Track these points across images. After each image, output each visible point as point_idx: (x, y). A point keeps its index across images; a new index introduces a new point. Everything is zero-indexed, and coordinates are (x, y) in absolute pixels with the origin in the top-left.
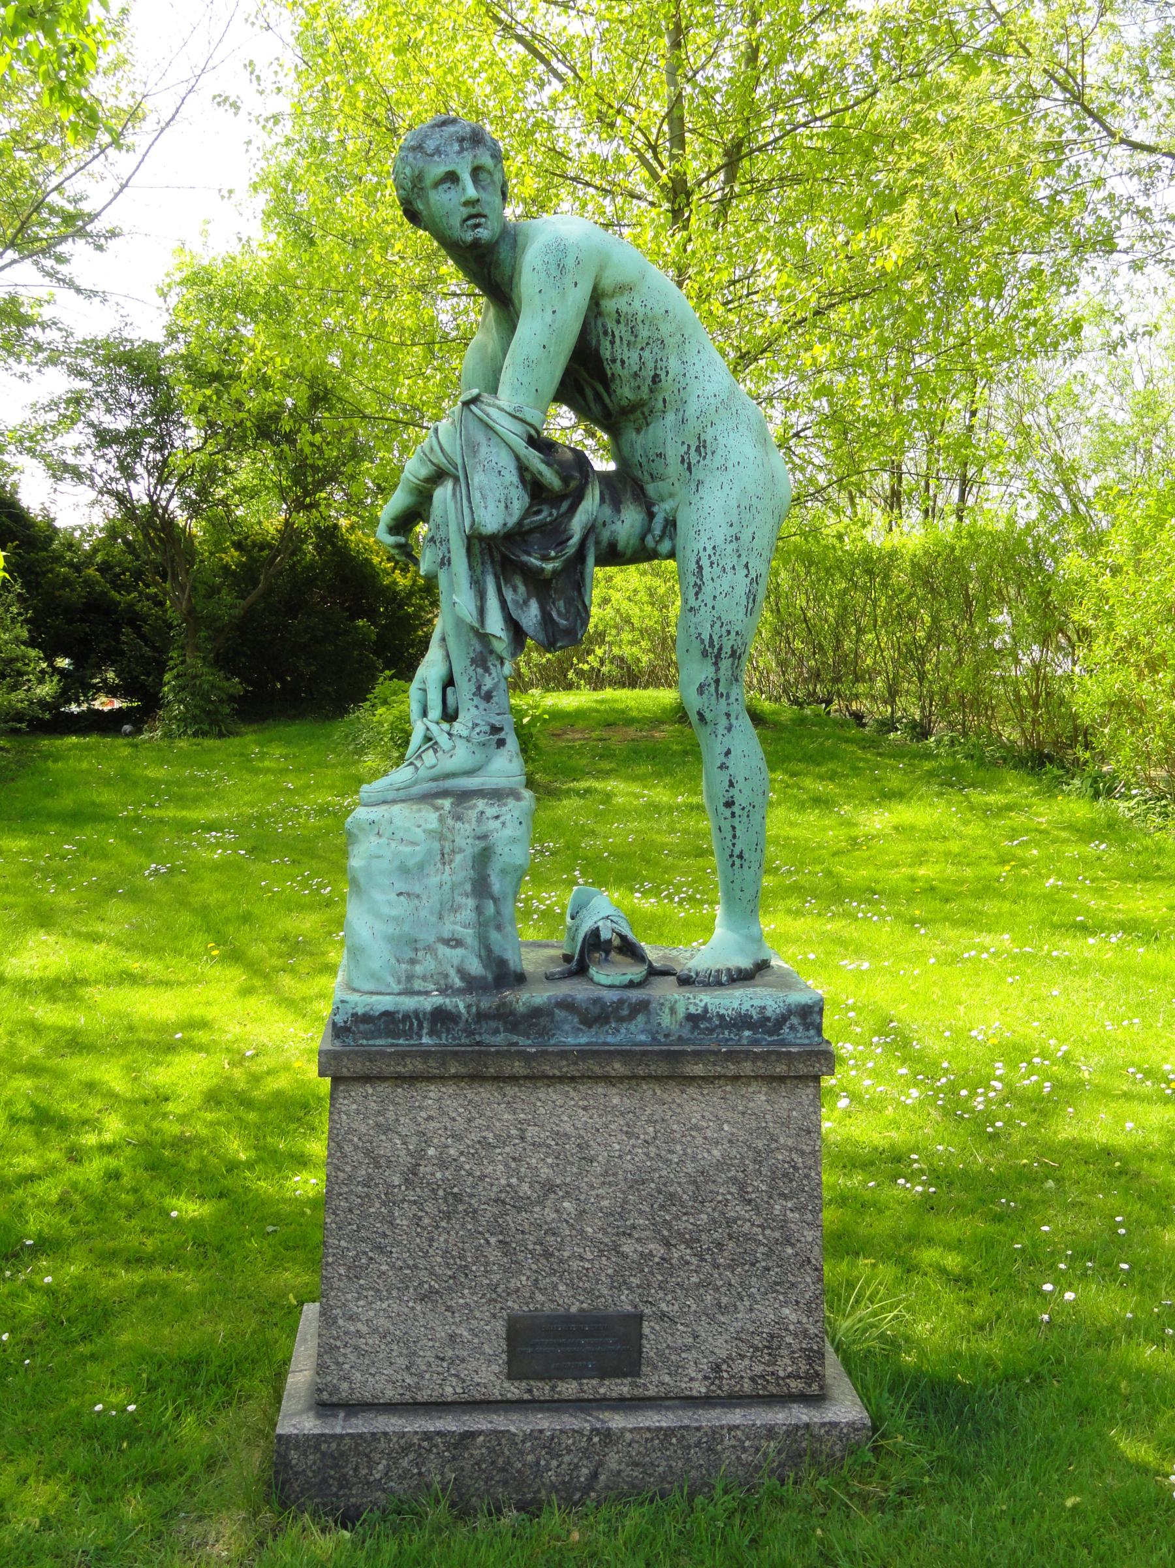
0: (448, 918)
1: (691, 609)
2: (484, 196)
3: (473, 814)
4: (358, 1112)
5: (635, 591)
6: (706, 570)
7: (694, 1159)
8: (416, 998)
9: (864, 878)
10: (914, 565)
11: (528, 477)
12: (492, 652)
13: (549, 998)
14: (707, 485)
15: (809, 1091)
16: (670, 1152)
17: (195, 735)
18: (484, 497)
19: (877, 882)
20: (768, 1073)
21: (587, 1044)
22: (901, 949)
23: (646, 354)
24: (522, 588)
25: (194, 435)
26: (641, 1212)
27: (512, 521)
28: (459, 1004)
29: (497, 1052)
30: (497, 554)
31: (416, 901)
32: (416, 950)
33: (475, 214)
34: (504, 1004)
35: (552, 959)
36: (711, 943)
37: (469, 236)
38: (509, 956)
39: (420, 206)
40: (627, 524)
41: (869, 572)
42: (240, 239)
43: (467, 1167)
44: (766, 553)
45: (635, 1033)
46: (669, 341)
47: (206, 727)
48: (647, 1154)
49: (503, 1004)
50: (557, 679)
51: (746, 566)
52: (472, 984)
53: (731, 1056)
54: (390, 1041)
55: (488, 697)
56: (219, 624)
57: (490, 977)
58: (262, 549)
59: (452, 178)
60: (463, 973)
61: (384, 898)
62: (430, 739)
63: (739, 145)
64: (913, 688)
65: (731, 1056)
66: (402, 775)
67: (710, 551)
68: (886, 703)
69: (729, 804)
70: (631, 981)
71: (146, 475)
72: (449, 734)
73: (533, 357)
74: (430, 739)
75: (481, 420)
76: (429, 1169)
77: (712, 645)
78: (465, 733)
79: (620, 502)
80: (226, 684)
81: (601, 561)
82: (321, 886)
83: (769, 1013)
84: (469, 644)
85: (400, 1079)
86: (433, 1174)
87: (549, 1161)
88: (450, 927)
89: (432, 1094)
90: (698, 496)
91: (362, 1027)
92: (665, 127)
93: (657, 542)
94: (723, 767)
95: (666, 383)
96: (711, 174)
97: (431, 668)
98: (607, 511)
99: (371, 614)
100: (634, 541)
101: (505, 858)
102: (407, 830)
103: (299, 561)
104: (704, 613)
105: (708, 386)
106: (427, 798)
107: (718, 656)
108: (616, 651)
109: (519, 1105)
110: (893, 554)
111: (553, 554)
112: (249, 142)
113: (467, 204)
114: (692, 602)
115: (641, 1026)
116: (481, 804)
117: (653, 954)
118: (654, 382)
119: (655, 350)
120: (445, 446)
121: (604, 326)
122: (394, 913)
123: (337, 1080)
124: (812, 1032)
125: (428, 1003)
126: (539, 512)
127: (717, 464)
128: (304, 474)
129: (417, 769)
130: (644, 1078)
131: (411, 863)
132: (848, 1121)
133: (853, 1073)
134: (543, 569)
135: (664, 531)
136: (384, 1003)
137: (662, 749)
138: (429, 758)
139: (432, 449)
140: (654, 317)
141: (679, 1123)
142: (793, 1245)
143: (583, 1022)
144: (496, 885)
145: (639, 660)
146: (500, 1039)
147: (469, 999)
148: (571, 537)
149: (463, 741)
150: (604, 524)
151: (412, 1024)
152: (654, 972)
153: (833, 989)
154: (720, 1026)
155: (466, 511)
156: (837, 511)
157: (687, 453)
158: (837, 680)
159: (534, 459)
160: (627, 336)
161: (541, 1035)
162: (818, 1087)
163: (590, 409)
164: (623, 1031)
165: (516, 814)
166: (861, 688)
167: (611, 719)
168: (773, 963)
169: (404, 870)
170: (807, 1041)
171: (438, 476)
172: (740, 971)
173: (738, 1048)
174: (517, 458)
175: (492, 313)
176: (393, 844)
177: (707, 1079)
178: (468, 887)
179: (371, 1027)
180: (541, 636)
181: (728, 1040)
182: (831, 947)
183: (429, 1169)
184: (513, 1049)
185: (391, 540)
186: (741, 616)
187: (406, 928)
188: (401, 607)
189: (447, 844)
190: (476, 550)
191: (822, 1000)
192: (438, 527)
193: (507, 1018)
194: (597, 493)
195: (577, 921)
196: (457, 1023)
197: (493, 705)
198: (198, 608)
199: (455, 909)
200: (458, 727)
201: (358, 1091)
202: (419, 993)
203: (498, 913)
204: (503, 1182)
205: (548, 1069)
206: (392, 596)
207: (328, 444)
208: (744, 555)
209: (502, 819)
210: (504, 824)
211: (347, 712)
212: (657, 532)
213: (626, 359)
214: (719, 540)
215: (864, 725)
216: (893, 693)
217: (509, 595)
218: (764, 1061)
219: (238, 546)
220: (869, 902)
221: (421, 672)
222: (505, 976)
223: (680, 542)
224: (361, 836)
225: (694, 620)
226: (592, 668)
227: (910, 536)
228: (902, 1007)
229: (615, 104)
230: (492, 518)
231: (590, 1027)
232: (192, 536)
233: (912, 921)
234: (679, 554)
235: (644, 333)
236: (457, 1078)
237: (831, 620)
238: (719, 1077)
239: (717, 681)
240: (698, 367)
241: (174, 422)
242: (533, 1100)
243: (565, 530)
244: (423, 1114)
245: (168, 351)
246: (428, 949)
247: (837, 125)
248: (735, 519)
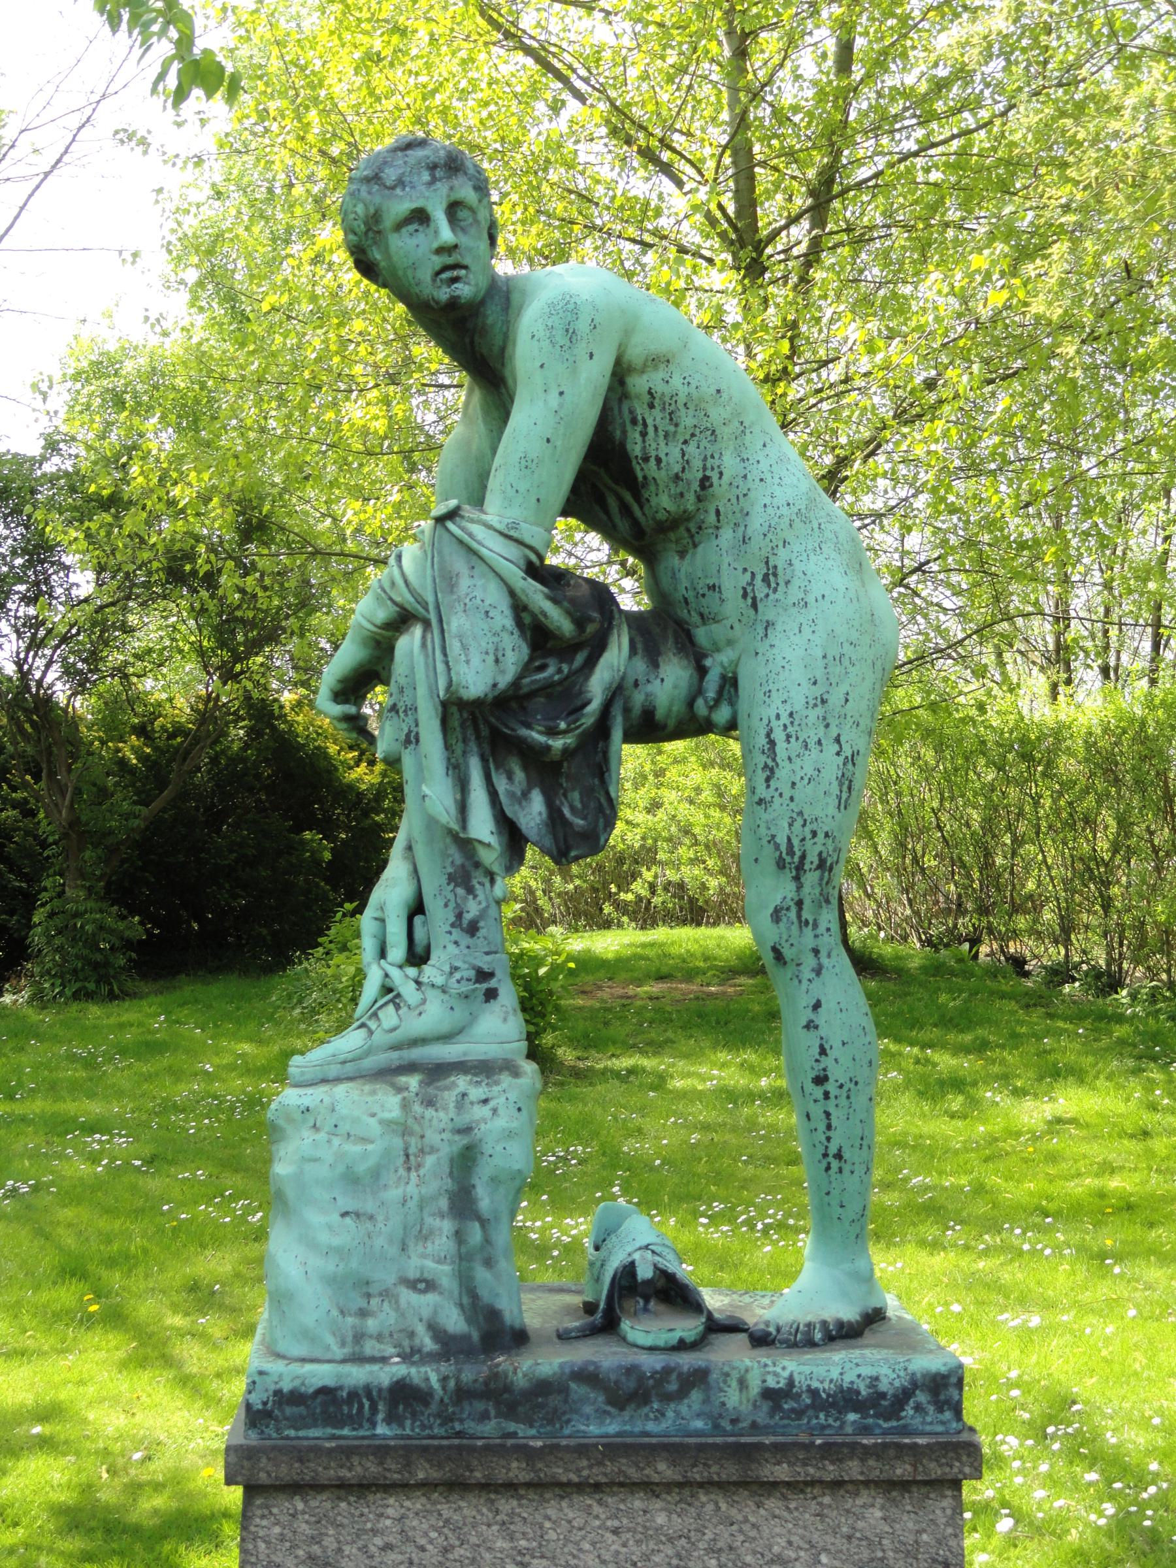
0: (415, 1249)
1: (760, 802)
2: (464, 240)
3: (450, 1097)
4: (282, 1538)
5: (698, 790)
6: (781, 746)
8: (368, 1367)
9: (1031, 1194)
10: (1088, 746)
11: (527, 619)
12: (477, 865)
13: (561, 1366)
14: (779, 627)
17: (76, 996)
18: (465, 648)
19: (1050, 1199)
20: (884, 1476)
21: (619, 1434)
22: (1086, 1297)
23: (691, 449)
24: (520, 775)
25: (84, 583)
27: (505, 681)
28: (430, 1376)
29: (487, 1448)
30: (484, 726)
31: (369, 1225)
32: (369, 1296)
33: (452, 265)
34: (496, 1375)
35: (568, 1311)
36: (795, 1283)
37: (443, 294)
38: (504, 1305)
39: (376, 255)
40: (669, 683)
41: (1026, 757)
42: (147, 319)
44: (865, 722)
45: (686, 1417)
46: (725, 432)
47: (91, 986)
49: (495, 1376)
50: (587, 912)
51: (838, 740)
52: (450, 1347)
53: (830, 1451)
54: (330, 1431)
55: (472, 929)
56: (110, 840)
57: (475, 1336)
58: (172, 736)
59: (420, 217)
60: (435, 1330)
61: (321, 1219)
62: (390, 990)
63: (830, 182)
64: (1094, 921)
65: (830, 1451)
66: (351, 1041)
67: (785, 719)
68: (1056, 942)
69: (820, 1080)
70: (681, 1341)
71: (14, 637)
72: (418, 982)
73: (533, 455)
74: (390, 990)
75: (461, 542)
77: (791, 852)
78: (439, 980)
79: (659, 654)
80: (121, 925)
81: (631, 737)
82: (248, 1211)
83: (884, 1386)
84: (444, 855)
85: (343, 1488)
88: (419, 1262)
90: (767, 642)
91: (289, 1410)
92: (727, 160)
93: (711, 709)
94: (810, 1026)
95: (720, 488)
96: (793, 220)
97: (391, 890)
98: (640, 666)
99: (327, 828)
100: (678, 708)
101: (498, 1160)
102: (356, 1121)
103: (223, 752)
104: (779, 807)
105: (778, 491)
106: (386, 1074)
107: (800, 868)
108: (672, 875)
109: (518, 1527)
110: (1059, 732)
111: (563, 725)
112: (160, 191)
113: (440, 251)
114: (762, 791)
115: (696, 1407)
116: (462, 1082)
117: (713, 1300)
119: (704, 443)
120: (412, 578)
121: (631, 412)
122: (336, 1241)
123: (252, 1491)
124: (948, 1415)
125: (385, 1375)
126: (543, 668)
127: (792, 599)
128: (233, 632)
129: (371, 1032)
130: (701, 1485)
131: (361, 1168)
132: (1013, 1553)
133: (1019, 1480)
134: (548, 748)
135: (720, 692)
136: (321, 1374)
137: (733, 1009)
138: (389, 1016)
139: (393, 584)
140: (702, 399)
141: (755, 1553)
143: (610, 1402)
144: (485, 1200)
145: (704, 887)
146: (489, 1428)
147: (446, 1368)
148: (588, 702)
149: (437, 992)
150: (636, 684)
151: (361, 1406)
152: (718, 1327)
153: (987, 1355)
154: (813, 1406)
155: (440, 667)
156: (980, 672)
157: (751, 584)
158: (984, 910)
159: (536, 594)
160: (664, 425)
161: (551, 1422)
162: (958, 1498)
163: (614, 526)
164: (670, 1414)
165: (513, 1096)
166: (1022, 922)
167: (665, 970)
168: (890, 1313)
169: (351, 1179)
170: (940, 1428)
171: (402, 620)
172: (840, 1324)
173: (839, 1439)
174: (512, 593)
175: (477, 396)
176: (336, 1141)
177: (795, 1487)
178: (444, 1203)
179: (302, 1410)
180: (548, 842)
182: (983, 1295)
184: (510, 1442)
185: (338, 709)
186: (832, 810)
187: (354, 1264)
188: (366, 814)
189: (413, 1141)
190: (455, 722)
191: (961, 1366)
192: (401, 690)
193: (500, 1396)
194: (625, 641)
195: (603, 1253)
196: (427, 1404)
197: (479, 941)
198: (84, 818)
199: (425, 1236)
200: (430, 972)
201: (283, 1506)
202: (373, 1360)
203: (487, 1241)
205: (559, 1472)
206: (350, 796)
207: (265, 589)
208: (834, 723)
209: (492, 1104)
210: (495, 1111)
211: (291, 962)
212: (711, 694)
213: (661, 455)
214: (798, 704)
215: (1027, 974)
216: (1066, 930)
217: (501, 784)
218: (878, 1458)
219: (142, 731)
220: (1039, 1229)
221: (377, 895)
222: (498, 1334)
223: (743, 706)
224: (289, 1130)
225: (765, 816)
226: (639, 899)
227: (1089, 706)
228: (1089, 1382)
229: (658, 132)
230: (477, 678)
231: (622, 1409)
232: (74, 722)
233: (1102, 1255)
234: (742, 721)
235: (687, 420)
236: (427, 1486)
237: (976, 826)
238: (812, 1483)
239: (800, 904)
240: (764, 466)
241: (53, 564)
242: (539, 1518)
243: (581, 693)
244: (378, 1541)
245: (49, 468)
246: (385, 1294)
247: (963, 153)
248: (819, 674)
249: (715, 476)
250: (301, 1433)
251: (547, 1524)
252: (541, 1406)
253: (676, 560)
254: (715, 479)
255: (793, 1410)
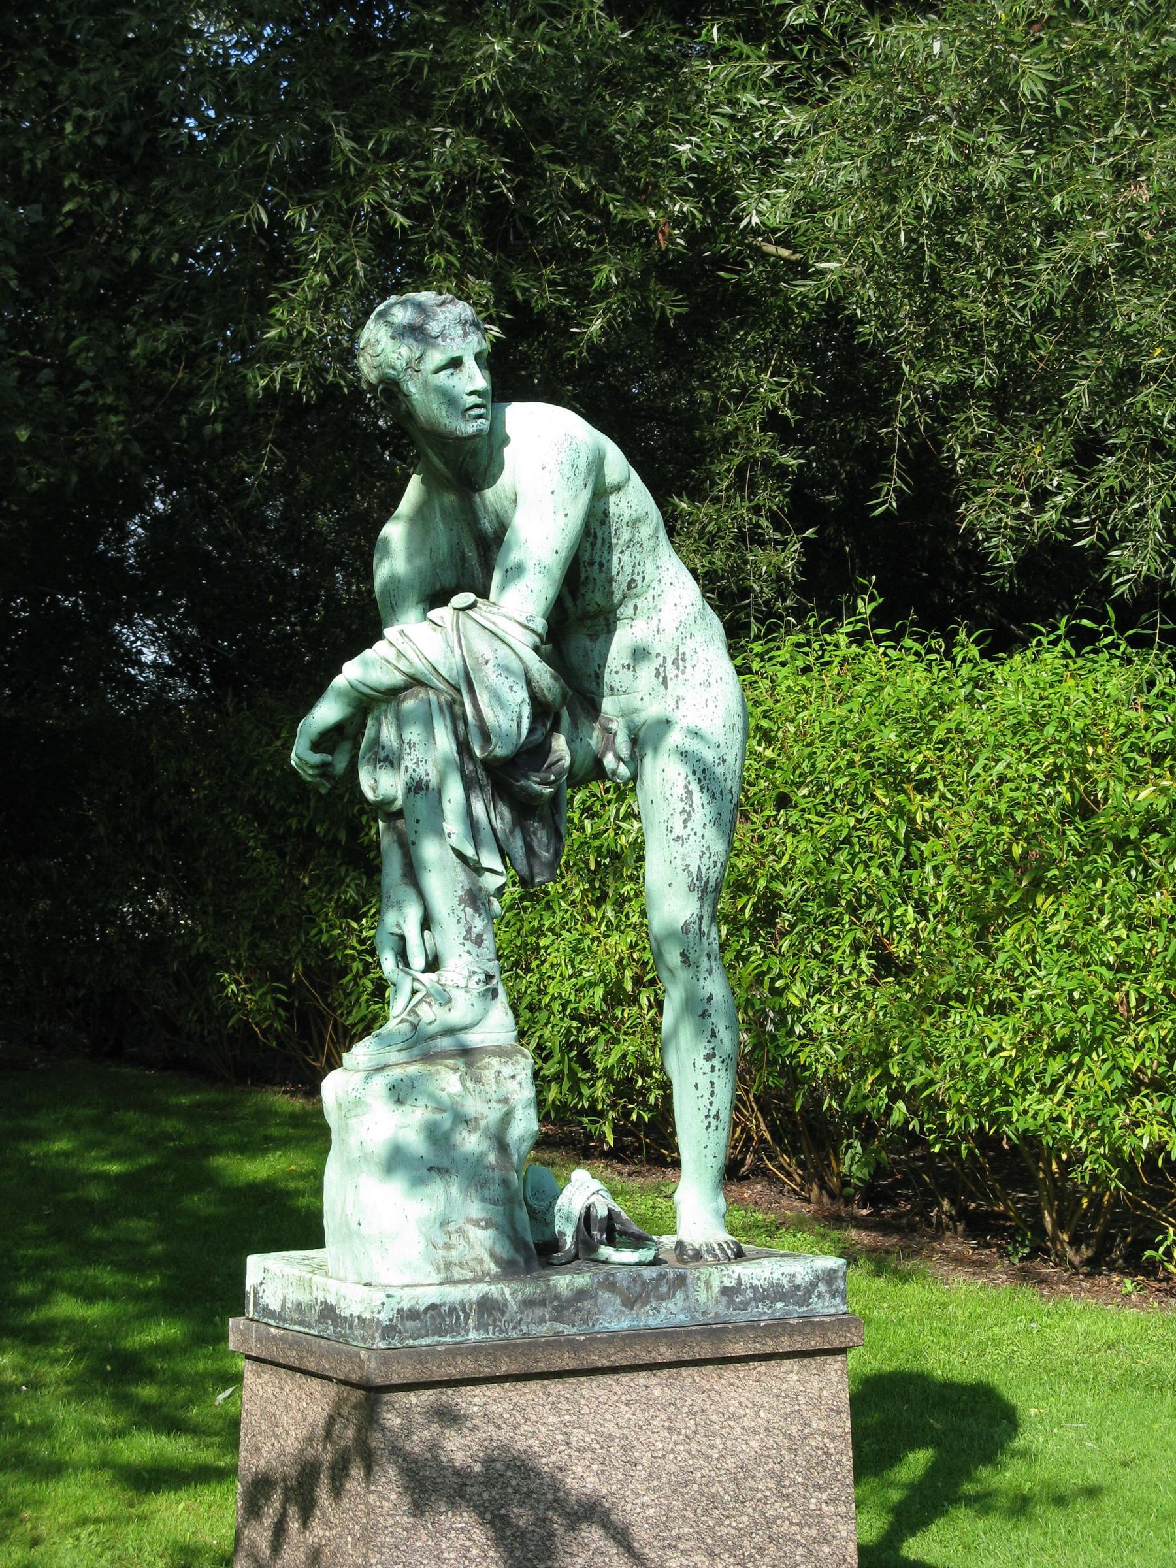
7: (734, 1454)
8: (461, 1287)
15: (837, 1366)
16: (711, 1446)
26: (685, 1519)
29: (548, 1343)
43: (514, 1483)
45: (671, 1312)
48: (689, 1452)
54: (437, 1338)
76: (475, 1489)
83: (798, 1282)
86: (480, 1495)
87: (595, 1467)
89: (476, 1400)
91: (409, 1324)
118: (629, 587)
119: (635, 554)
141: (718, 1412)
142: (829, 1543)
151: (458, 1317)
154: (754, 1299)
157: (663, 666)
164: (663, 1311)
170: (833, 1311)
179: (417, 1323)
181: (761, 1312)
183: (475, 1489)
196: (503, 1313)
204: (550, 1497)
209: (518, 1078)
231: (632, 1308)
249: (639, 578)
250: (417, 1342)
251: (583, 1402)
252: (578, 1310)
253: (588, 642)
254: (639, 582)
255: (741, 1302)
